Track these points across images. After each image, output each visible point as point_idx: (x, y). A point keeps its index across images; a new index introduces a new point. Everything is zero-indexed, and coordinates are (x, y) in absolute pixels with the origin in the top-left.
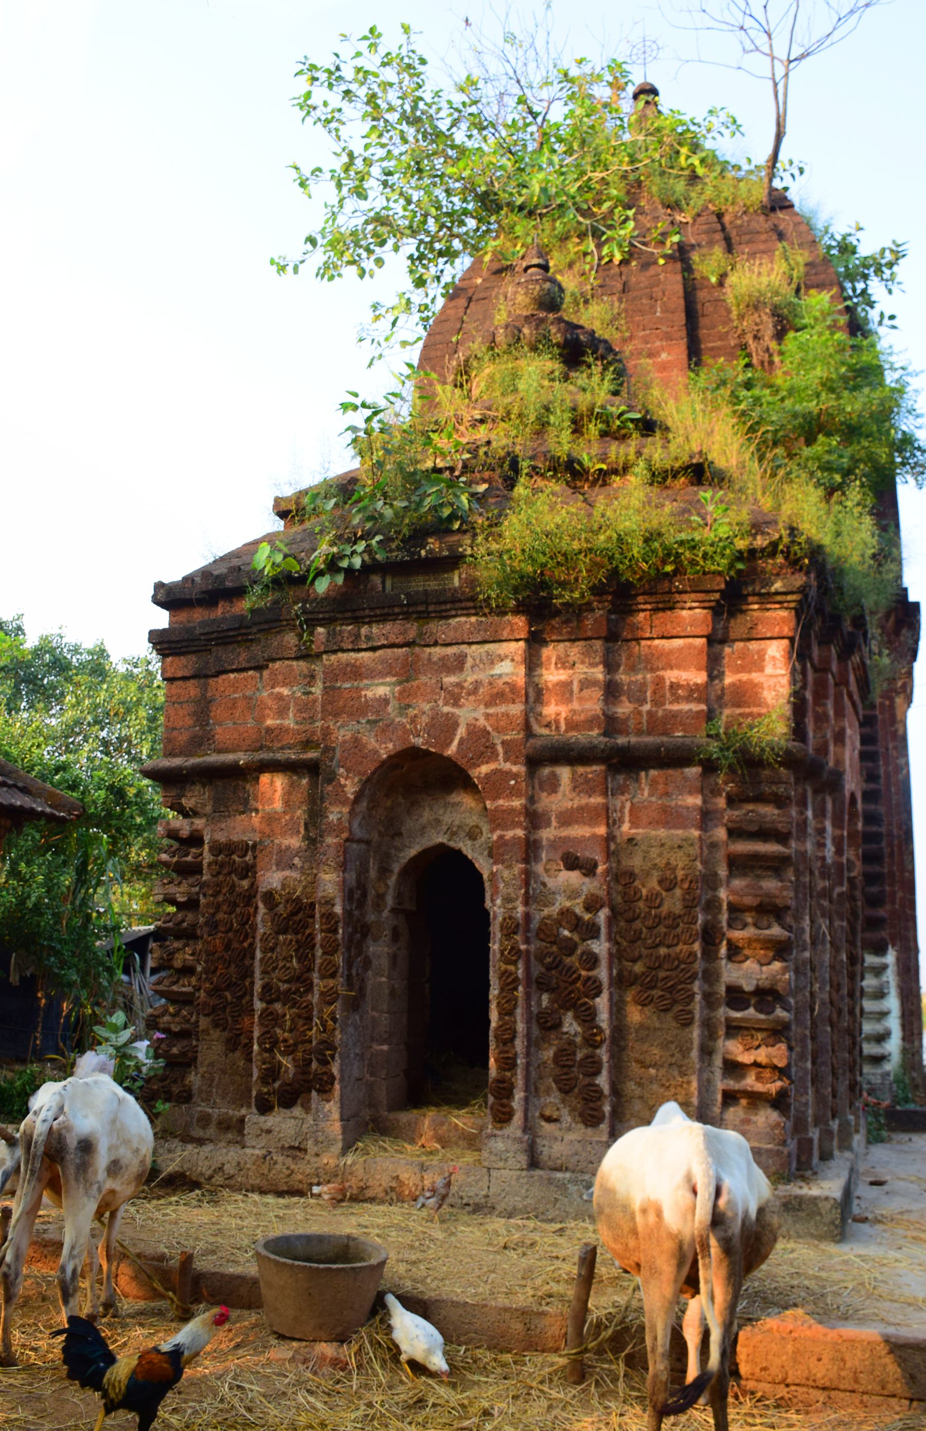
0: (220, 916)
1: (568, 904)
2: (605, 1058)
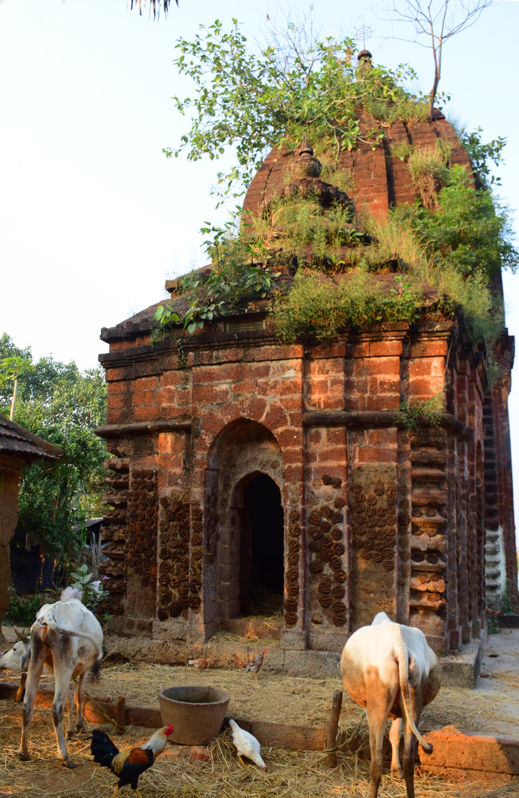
0: (139, 512)
1: (326, 504)
2: (346, 588)
